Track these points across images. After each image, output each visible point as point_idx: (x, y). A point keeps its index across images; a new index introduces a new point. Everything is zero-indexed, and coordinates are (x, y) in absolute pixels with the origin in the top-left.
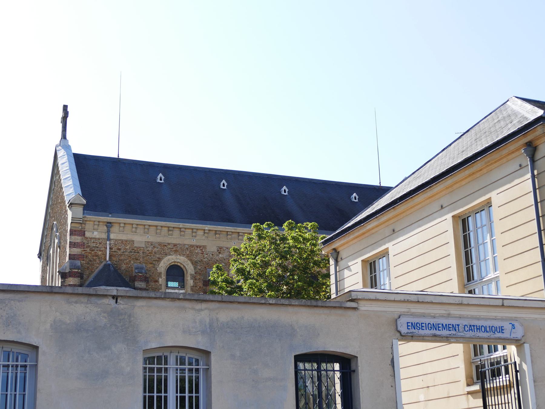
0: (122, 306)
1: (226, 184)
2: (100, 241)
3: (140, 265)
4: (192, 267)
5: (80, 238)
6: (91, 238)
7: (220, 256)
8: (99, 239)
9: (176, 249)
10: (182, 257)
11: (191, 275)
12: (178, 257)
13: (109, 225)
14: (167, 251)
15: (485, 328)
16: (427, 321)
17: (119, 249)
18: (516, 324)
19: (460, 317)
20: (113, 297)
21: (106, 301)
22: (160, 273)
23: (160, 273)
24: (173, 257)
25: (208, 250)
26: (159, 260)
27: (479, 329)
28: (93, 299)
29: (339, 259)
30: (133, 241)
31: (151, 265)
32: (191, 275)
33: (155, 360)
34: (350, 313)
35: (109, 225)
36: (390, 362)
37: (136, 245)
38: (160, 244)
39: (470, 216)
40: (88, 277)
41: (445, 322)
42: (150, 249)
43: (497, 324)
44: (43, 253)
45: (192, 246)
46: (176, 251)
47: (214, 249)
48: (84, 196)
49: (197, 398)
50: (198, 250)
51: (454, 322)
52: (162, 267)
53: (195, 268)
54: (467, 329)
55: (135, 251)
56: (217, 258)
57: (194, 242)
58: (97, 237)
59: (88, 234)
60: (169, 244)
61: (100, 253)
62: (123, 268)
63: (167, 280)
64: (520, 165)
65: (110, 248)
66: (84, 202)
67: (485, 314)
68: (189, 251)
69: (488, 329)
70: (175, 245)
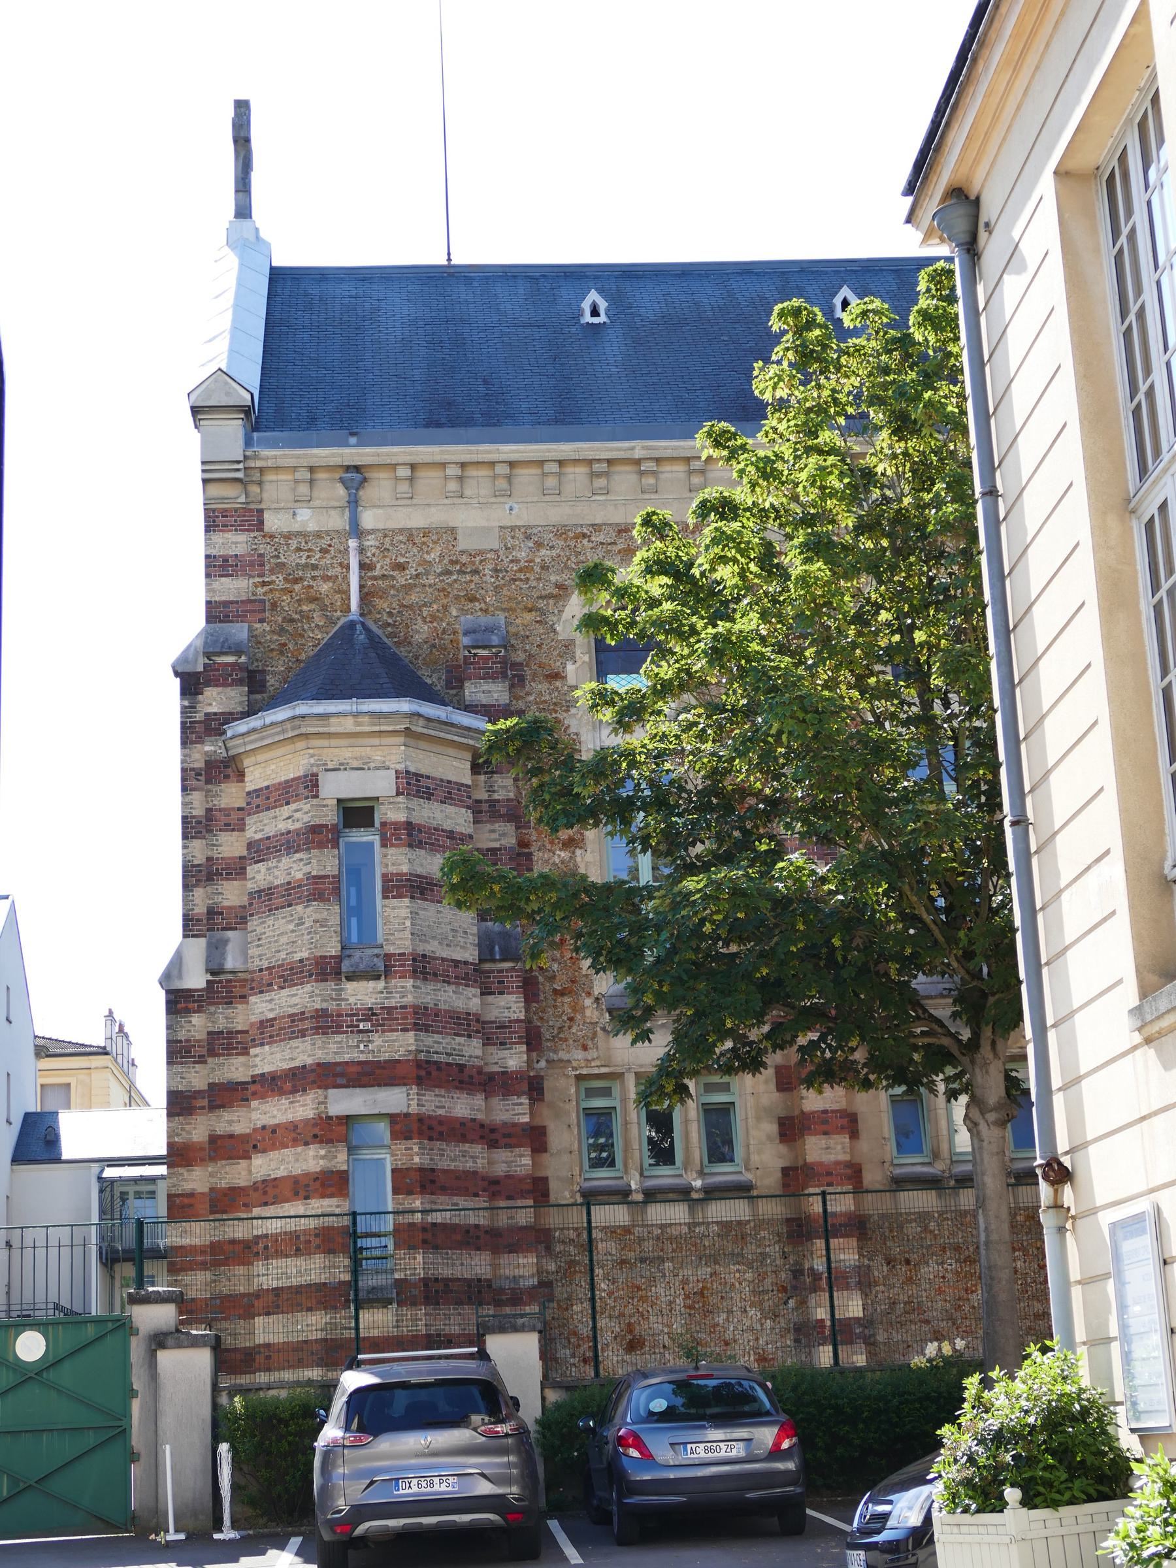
2: (324, 542)
5: (242, 537)
6: (288, 536)
8: (318, 535)
13: (355, 477)
17: (401, 567)
31: (529, 617)
37: (462, 544)
38: (561, 531)
42: (522, 555)
55: (465, 565)
58: (312, 527)
59: (274, 522)
60: (597, 528)
61: (325, 587)
65: (362, 566)
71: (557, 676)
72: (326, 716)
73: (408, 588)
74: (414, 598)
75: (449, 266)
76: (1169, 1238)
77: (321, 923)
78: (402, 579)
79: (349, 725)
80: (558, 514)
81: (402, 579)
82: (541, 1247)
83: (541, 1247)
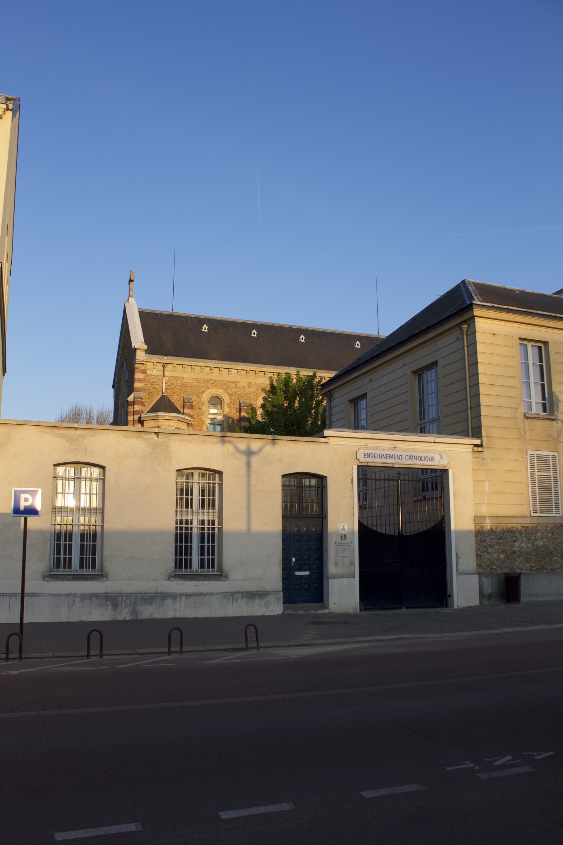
0: (162, 440)
1: (256, 333)
2: (158, 377)
3: (188, 396)
4: (228, 398)
5: (142, 375)
6: (151, 375)
7: (250, 389)
8: (157, 376)
9: (216, 383)
10: (220, 391)
11: (227, 404)
12: (218, 390)
13: (164, 365)
14: (209, 386)
15: (421, 458)
16: (379, 452)
17: (172, 384)
18: (444, 456)
19: (403, 450)
20: (156, 433)
21: (149, 436)
22: (203, 403)
23: (203, 403)
24: (214, 390)
25: (240, 385)
26: (203, 392)
27: (416, 458)
28: (143, 435)
29: (332, 399)
30: (183, 378)
31: (196, 396)
32: (227, 404)
33: (185, 473)
34: (323, 445)
35: (164, 365)
36: (350, 481)
37: (185, 381)
38: (203, 380)
39: (364, 396)
40: (149, 405)
41: (392, 453)
42: (196, 384)
43: (429, 455)
44: (116, 385)
45: (229, 382)
46: (216, 386)
47: (246, 384)
48: (146, 343)
49: (192, 499)
50: (233, 385)
51: (399, 453)
52: (206, 397)
53: (230, 399)
54: (407, 458)
55: (184, 385)
56: (248, 391)
57: (230, 379)
58: (156, 374)
59: (149, 372)
60: (210, 380)
61: (158, 387)
62: (175, 399)
63: (209, 408)
64: (458, 338)
65: (166, 383)
66: (146, 347)
67: (421, 448)
68: (226, 385)
69: (423, 459)
70: (215, 381)
71: (201, 409)
72: (164, 416)
73: (174, 388)
74: (174, 390)
75: (249, 533)
76: (327, 550)
77: (254, 411)
78: (173, 386)
79: (167, 418)
80: (203, 377)
81: (173, 386)
82: (219, 406)
83: (219, 406)
